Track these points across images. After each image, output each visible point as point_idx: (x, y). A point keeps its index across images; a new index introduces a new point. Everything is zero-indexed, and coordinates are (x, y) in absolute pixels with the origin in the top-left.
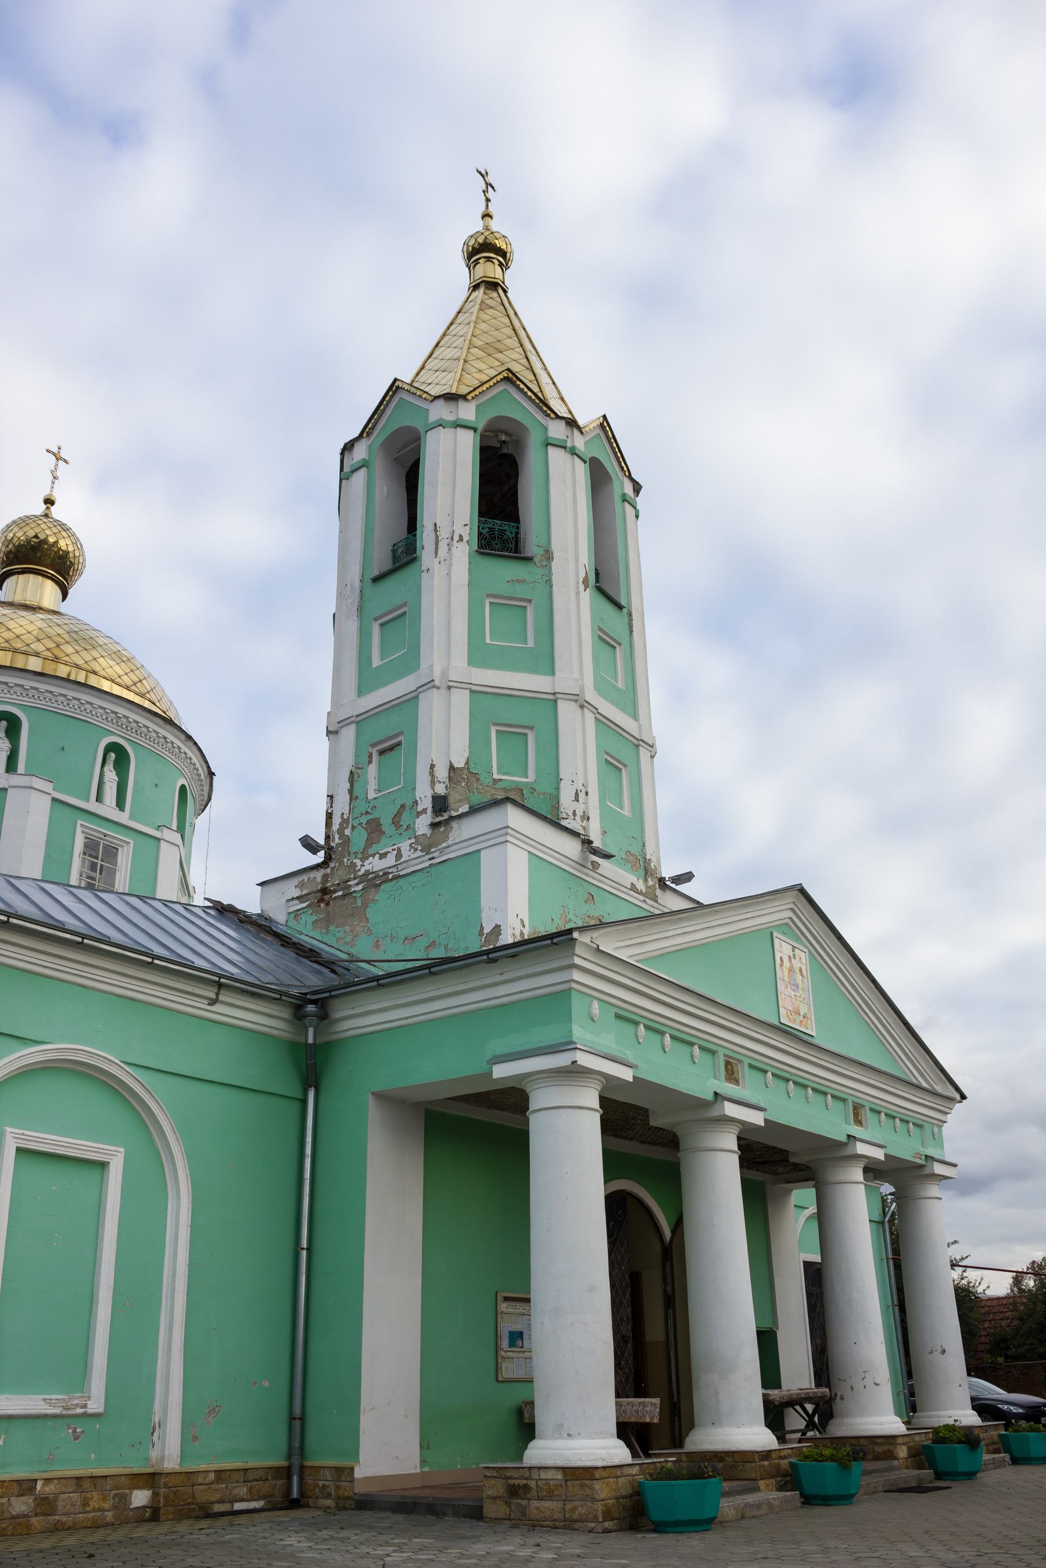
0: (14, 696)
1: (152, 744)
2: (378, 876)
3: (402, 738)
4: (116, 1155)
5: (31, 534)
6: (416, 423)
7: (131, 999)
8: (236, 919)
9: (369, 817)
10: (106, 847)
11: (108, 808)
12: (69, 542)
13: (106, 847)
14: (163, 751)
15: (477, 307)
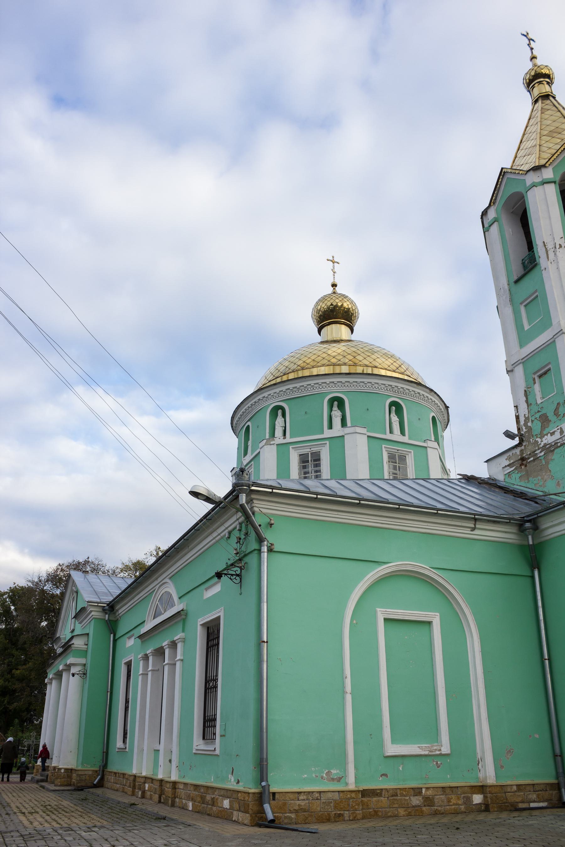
0: (338, 388)
1: (413, 398)
2: (551, 446)
3: (550, 366)
4: (435, 617)
5: (329, 304)
6: (520, 189)
7: (429, 534)
8: (477, 482)
9: (540, 414)
10: (399, 456)
11: (397, 436)
12: (349, 303)
13: (399, 456)
14: (420, 400)
15: (540, 112)
